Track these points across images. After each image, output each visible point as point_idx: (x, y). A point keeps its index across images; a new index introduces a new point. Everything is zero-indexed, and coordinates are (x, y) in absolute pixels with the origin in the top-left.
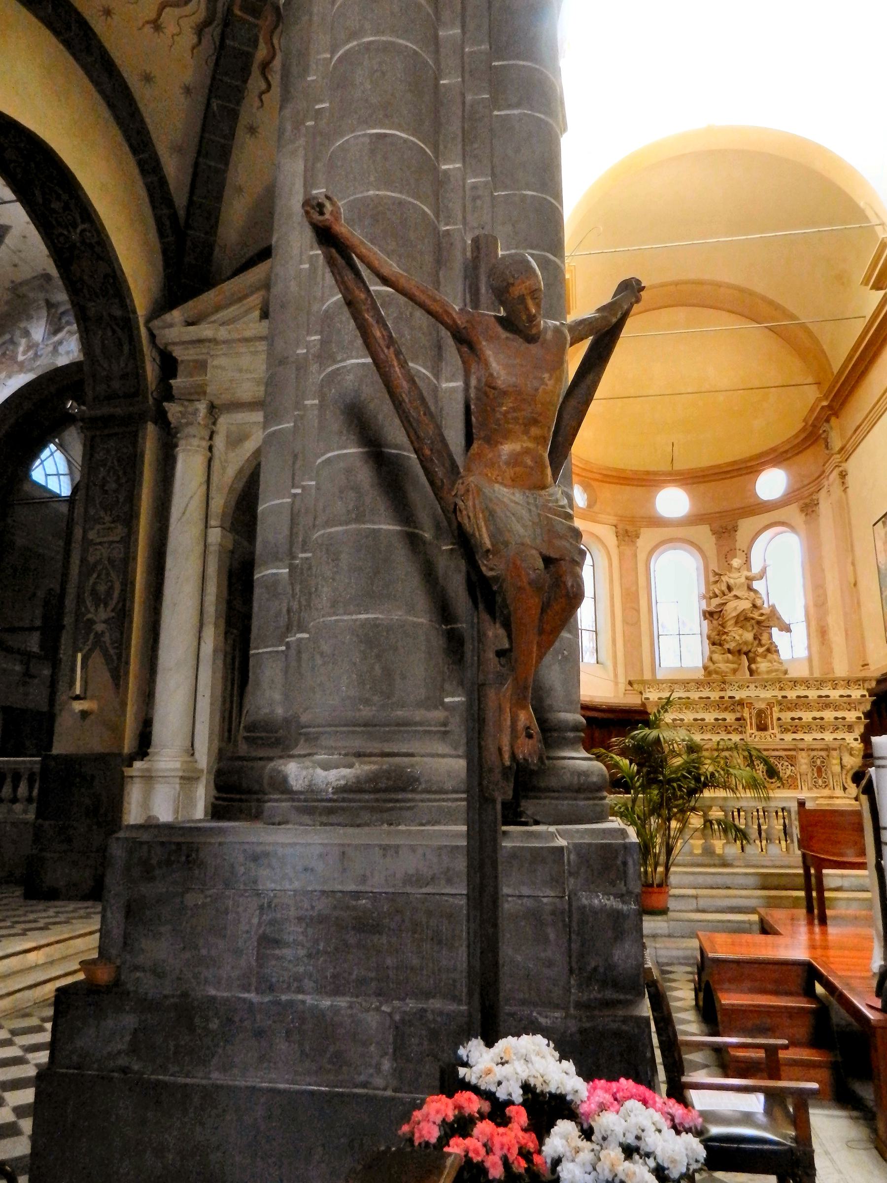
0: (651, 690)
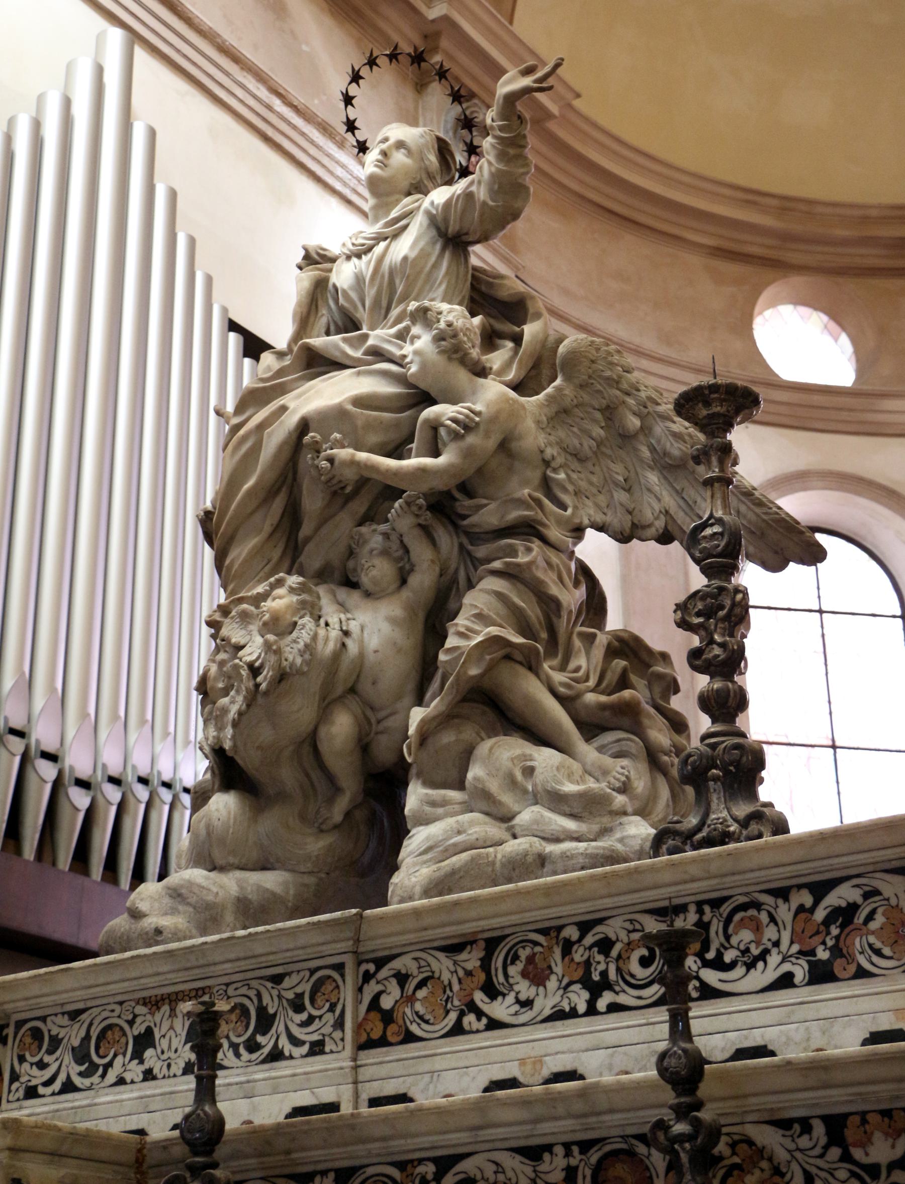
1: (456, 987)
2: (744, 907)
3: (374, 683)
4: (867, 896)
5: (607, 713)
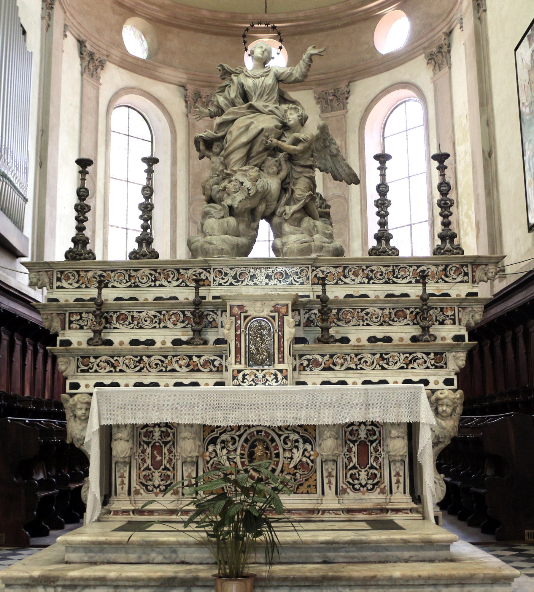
0: (64, 284)
1: (336, 275)
2: (403, 268)
3: (271, 197)
4: (428, 269)
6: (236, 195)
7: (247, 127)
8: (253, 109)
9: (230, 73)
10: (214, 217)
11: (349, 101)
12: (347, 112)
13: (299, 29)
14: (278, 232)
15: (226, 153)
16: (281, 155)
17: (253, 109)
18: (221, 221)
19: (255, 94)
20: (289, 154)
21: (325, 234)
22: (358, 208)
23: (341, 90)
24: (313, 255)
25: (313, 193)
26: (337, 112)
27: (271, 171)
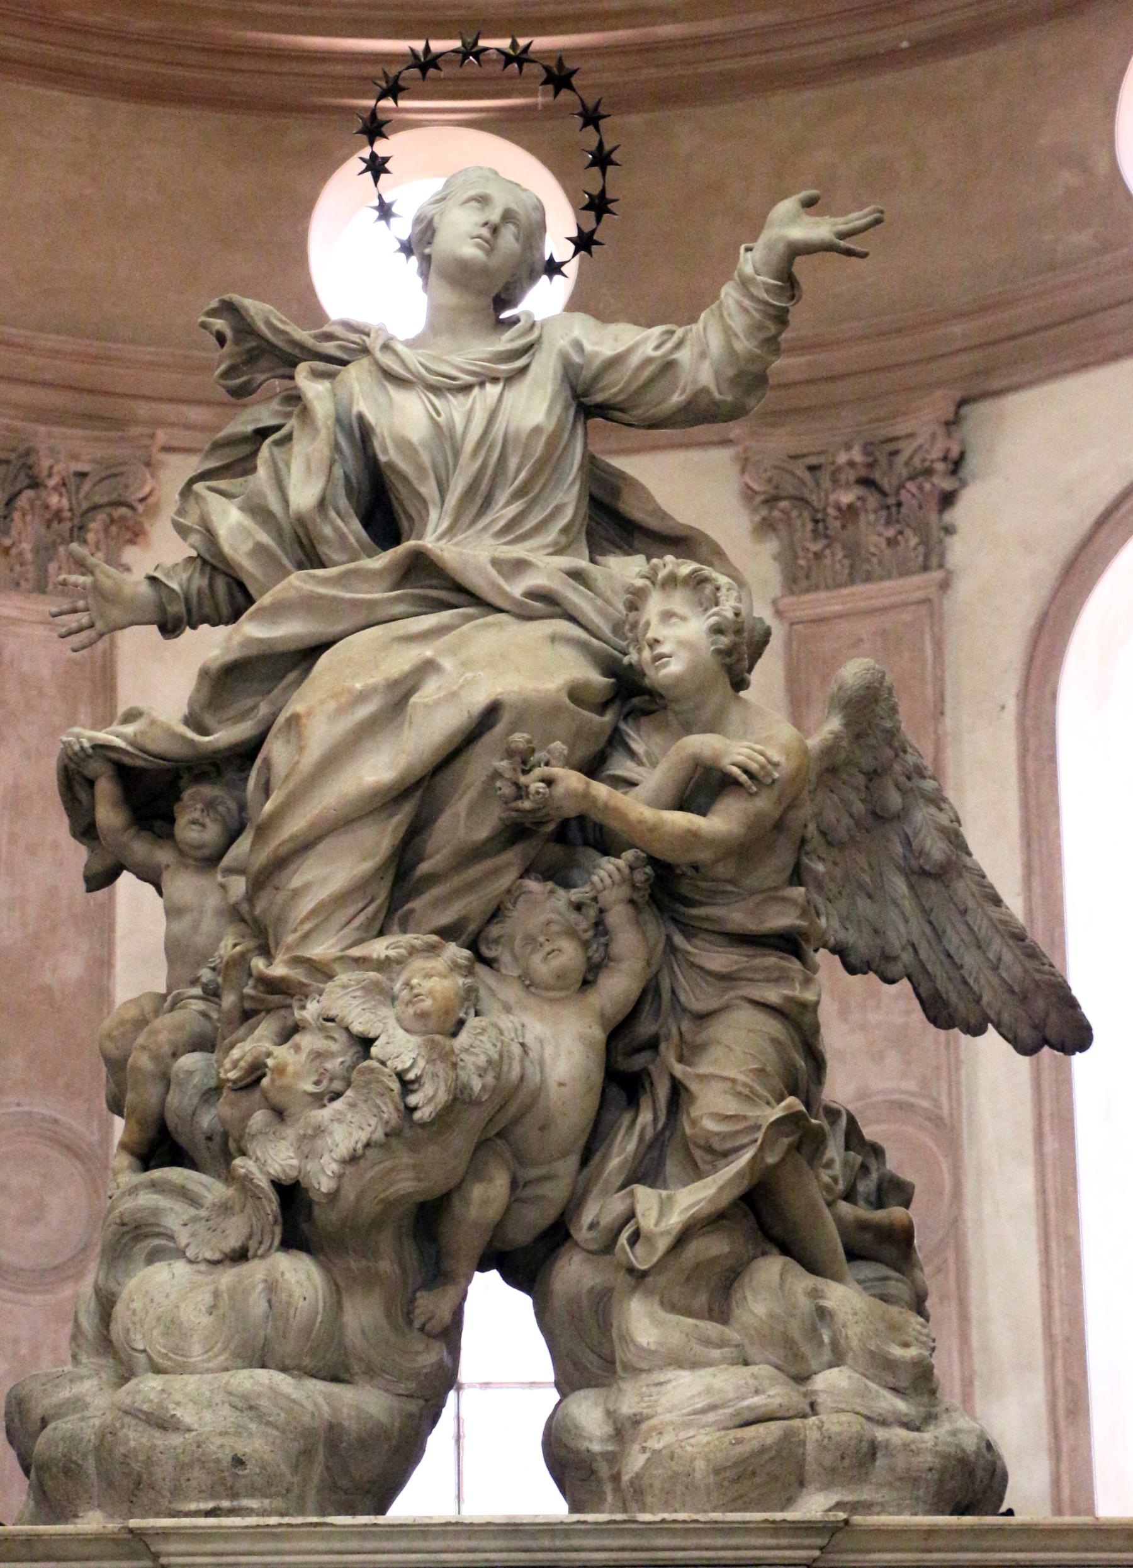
3: (542, 1128)
5: (868, 1236)
6: (324, 1114)
7: (399, 697)
8: (435, 586)
9: (287, 358)
10: (180, 1253)
11: (957, 514)
12: (945, 585)
13: (650, 73)
14: (584, 1353)
15: (263, 857)
16: (607, 872)
17: (435, 586)
18: (228, 1277)
19: (443, 490)
20: (652, 861)
21: (882, 1367)
22: (1025, 1183)
23: (907, 449)
24: (814, 1505)
25: (808, 1105)
26: (887, 584)
27: (542, 967)
